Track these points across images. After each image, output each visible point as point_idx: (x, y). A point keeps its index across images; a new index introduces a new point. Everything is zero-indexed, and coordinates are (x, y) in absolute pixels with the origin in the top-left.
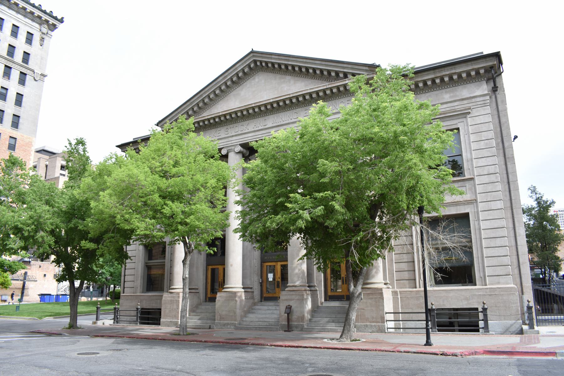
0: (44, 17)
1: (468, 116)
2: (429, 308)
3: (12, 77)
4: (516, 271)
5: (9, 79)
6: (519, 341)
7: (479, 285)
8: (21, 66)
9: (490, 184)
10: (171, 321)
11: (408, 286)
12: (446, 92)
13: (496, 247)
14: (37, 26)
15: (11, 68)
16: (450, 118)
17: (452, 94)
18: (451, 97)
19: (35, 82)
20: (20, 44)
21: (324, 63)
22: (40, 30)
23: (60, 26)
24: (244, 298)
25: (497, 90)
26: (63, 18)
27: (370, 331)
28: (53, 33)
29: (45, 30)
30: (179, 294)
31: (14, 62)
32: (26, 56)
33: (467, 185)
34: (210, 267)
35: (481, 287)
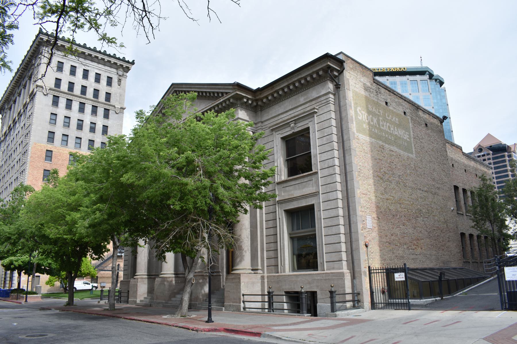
0: (119, 63)
1: (315, 115)
2: (507, 279)
3: (98, 114)
5: (96, 116)
8: (105, 104)
9: (329, 176)
11: (274, 271)
12: (302, 96)
13: (332, 235)
14: (115, 70)
15: (97, 107)
16: (303, 119)
17: (305, 97)
18: (304, 99)
19: (117, 115)
20: (103, 87)
21: (209, 87)
22: (117, 73)
23: (133, 68)
24: (174, 282)
25: (339, 88)
26: (134, 61)
27: (232, 310)
28: (128, 74)
29: (121, 73)
31: (99, 102)
32: (108, 96)
33: (313, 179)
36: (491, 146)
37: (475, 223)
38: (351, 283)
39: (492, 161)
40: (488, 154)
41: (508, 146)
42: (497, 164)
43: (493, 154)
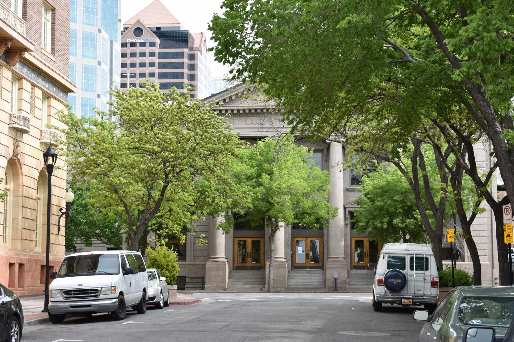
4: (490, 253)
6: (426, 318)
7: (467, 262)
10: (217, 286)
30: (225, 263)
34: (237, 239)
35: (468, 263)
36: (158, 28)
37: (210, 180)
38: (482, 279)
39: (156, 60)
40: (152, 44)
41: (190, 34)
42: (178, 63)
43: (161, 47)
